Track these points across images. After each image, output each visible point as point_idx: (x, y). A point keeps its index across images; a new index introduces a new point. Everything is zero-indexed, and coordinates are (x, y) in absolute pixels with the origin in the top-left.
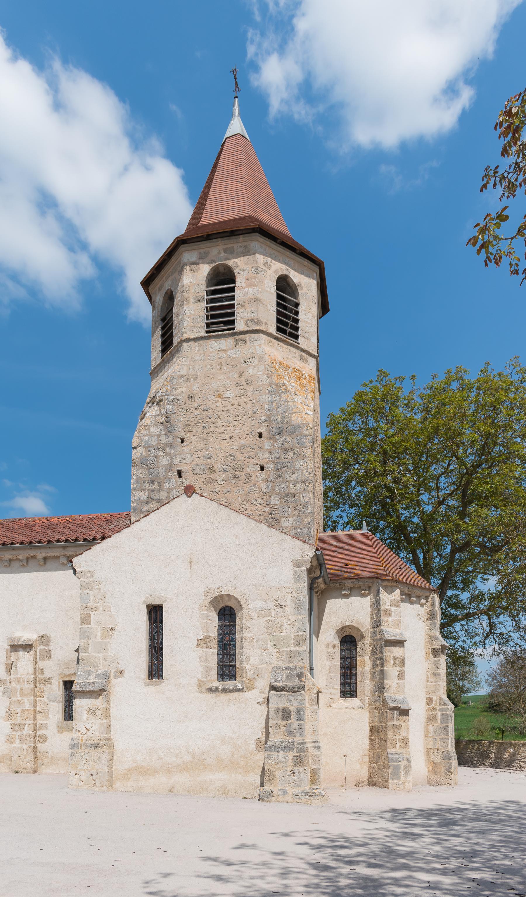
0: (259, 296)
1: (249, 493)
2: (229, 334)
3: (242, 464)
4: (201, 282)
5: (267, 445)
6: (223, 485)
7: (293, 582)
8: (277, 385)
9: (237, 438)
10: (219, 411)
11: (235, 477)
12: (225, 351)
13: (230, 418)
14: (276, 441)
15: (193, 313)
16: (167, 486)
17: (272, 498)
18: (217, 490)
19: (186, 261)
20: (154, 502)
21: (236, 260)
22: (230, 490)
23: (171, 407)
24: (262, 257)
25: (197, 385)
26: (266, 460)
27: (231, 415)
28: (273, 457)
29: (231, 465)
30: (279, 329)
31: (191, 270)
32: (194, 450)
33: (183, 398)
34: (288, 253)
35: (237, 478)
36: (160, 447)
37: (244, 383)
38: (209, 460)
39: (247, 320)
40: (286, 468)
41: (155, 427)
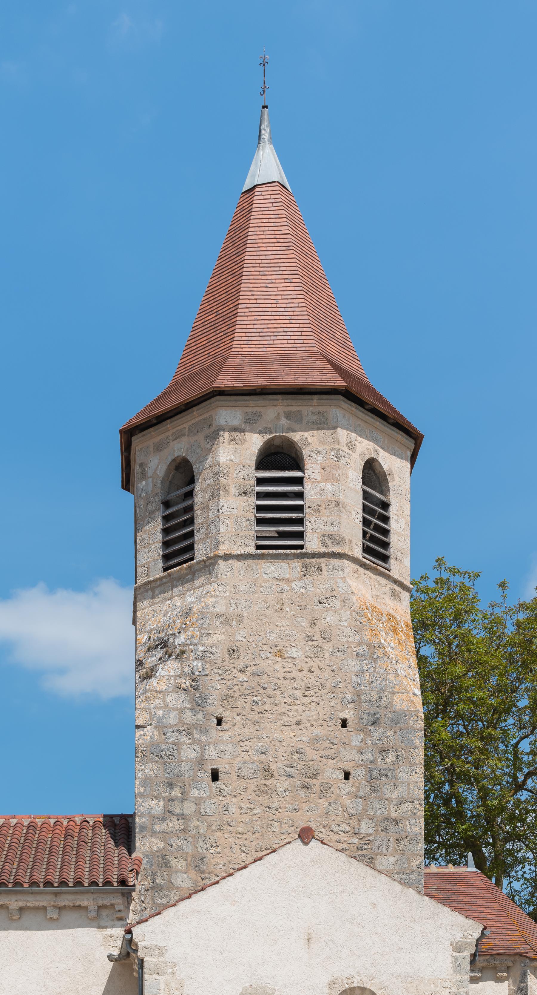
0: (342, 498)
1: (327, 814)
2: (294, 554)
3: (316, 767)
4: (248, 462)
5: (356, 739)
6: (286, 798)
7: (452, 972)
8: (370, 645)
9: (308, 725)
10: (279, 679)
11: (306, 787)
12: (288, 581)
13: (296, 692)
14: (369, 734)
15: (235, 511)
16: (194, 793)
17: (363, 824)
18: (276, 805)
19: (223, 423)
20: (174, 819)
21: (306, 434)
22: (297, 807)
23: (200, 664)
24: (345, 432)
25: (243, 633)
26: (352, 763)
27: (298, 687)
28: (365, 759)
29: (299, 767)
30: (367, 550)
31: (232, 439)
32: (238, 738)
33: (221, 652)
34: (378, 423)
35: (308, 788)
36: (182, 729)
37: (318, 636)
38: (263, 756)
39: (324, 536)
40: (384, 778)
41: (173, 695)
